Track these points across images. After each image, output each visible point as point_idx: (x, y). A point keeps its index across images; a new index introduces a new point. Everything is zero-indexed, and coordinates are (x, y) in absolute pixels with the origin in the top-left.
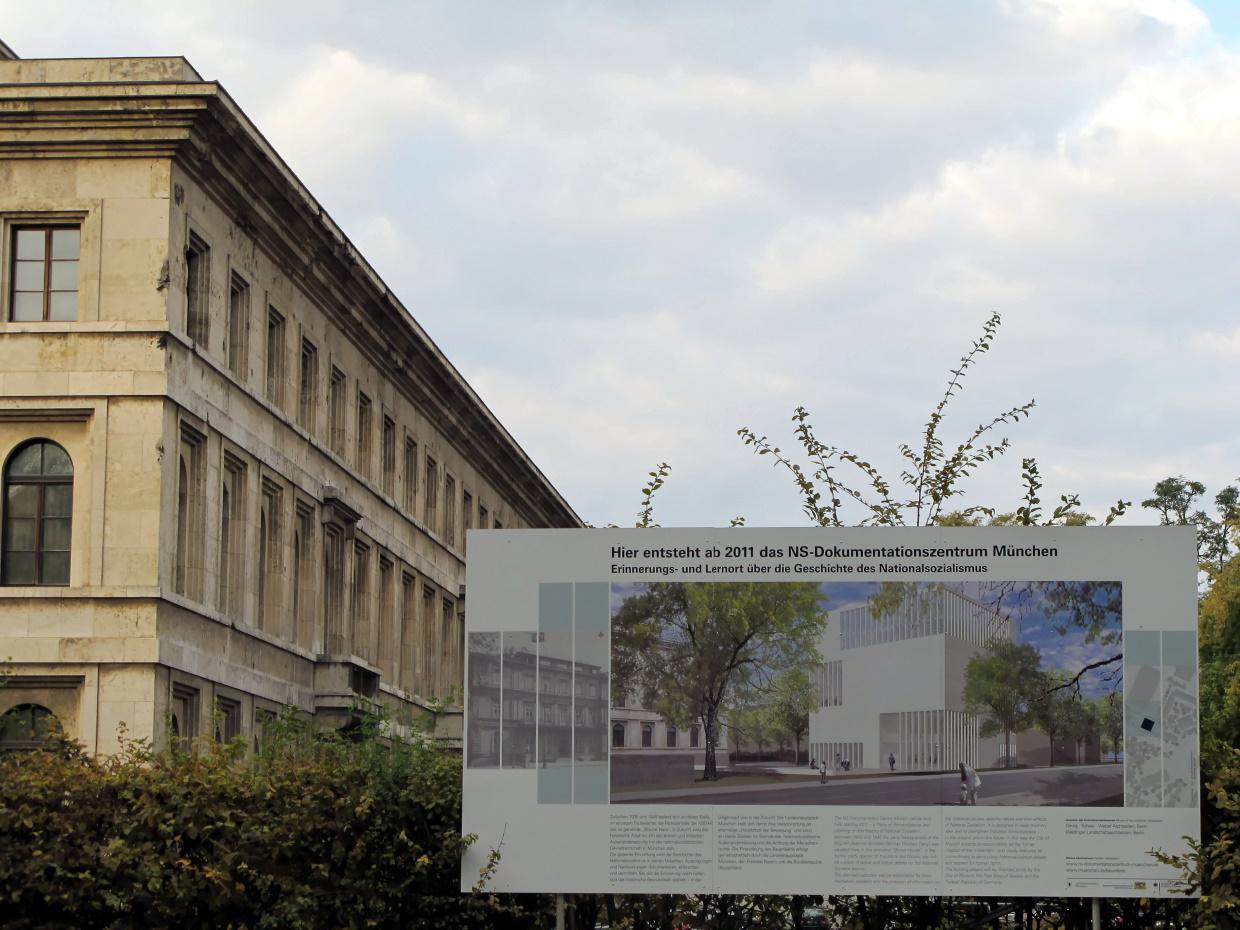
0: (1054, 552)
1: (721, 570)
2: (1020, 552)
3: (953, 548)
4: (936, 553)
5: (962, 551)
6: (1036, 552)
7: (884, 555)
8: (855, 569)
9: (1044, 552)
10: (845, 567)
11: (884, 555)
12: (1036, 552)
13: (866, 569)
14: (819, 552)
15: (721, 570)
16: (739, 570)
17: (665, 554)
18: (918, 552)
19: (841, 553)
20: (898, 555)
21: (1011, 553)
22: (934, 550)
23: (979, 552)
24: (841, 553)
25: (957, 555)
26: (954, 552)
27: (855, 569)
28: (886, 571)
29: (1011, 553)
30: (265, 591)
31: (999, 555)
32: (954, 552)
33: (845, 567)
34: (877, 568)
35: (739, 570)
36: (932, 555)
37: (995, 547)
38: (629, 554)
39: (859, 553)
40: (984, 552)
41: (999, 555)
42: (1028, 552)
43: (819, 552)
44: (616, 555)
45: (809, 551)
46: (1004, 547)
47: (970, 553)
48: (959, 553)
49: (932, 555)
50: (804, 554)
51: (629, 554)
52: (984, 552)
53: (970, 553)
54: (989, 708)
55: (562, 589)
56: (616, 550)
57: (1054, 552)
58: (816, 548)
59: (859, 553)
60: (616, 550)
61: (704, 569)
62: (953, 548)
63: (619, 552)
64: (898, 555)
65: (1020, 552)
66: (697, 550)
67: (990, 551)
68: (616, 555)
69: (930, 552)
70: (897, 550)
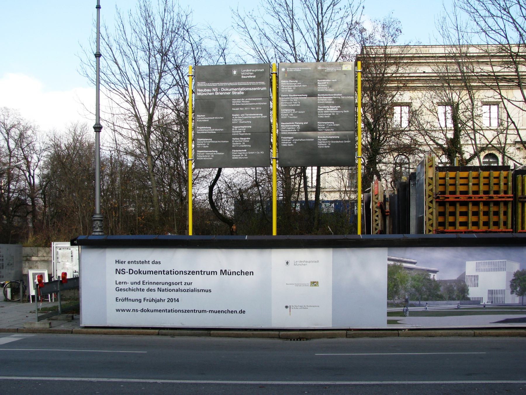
0: (252, 273)
1: (123, 283)
2: (234, 273)
3: (200, 271)
4: (191, 273)
5: (204, 272)
6: (243, 273)
7: (164, 274)
8: (146, 290)
9: (247, 273)
10: (140, 289)
11: (164, 274)
12: (243, 273)
13: (151, 290)
14: (131, 272)
15: (123, 283)
16: (180, 284)
17: (136, 263)
18: (181, 272)
19: (142, 272)
20: (171, 274)
21: (229, 274)
22: (190, 272)
23: (213, 273)
24: (142, 272)
25: (201, 274)
26: (200, 273)
27: (146, 290)
28: (161, 291)
29: (229, 274)
30: (409, 260)
31: (223, 274)
32: (200, 273)
33: (140, 289)
34: (156, 290)
35: (180, 284)
36: (188, 274)
37: (221, 271)
38: (122, 262)
39: (151, 272)
40: (215, 273)
41: (223, 274)
42: (239, 273)
43: (131, 272)
44: (117, 263)
45: (125, 271)
46: (226, 271)
47: (208, 273)
48: (203, 273)
49: (188, 274)
50: (123, 273)
51: (122, 262)
52: (215, 273)
53: (208, 273)
54: (359, 51)
55: (388, 304)
56: (117, 261)
57: (252, 273)
58: (130, 270)
59: (151, 272)
60: (117, 261)
61: (141, 283)
62: (200, 271)
63: (118, 262)
64: (171, 274)
65: (234, 273)
66: (149, 261)
67: (219, 273)
68: (117, 263)
69: (188, 272)
70: (171, 271)
